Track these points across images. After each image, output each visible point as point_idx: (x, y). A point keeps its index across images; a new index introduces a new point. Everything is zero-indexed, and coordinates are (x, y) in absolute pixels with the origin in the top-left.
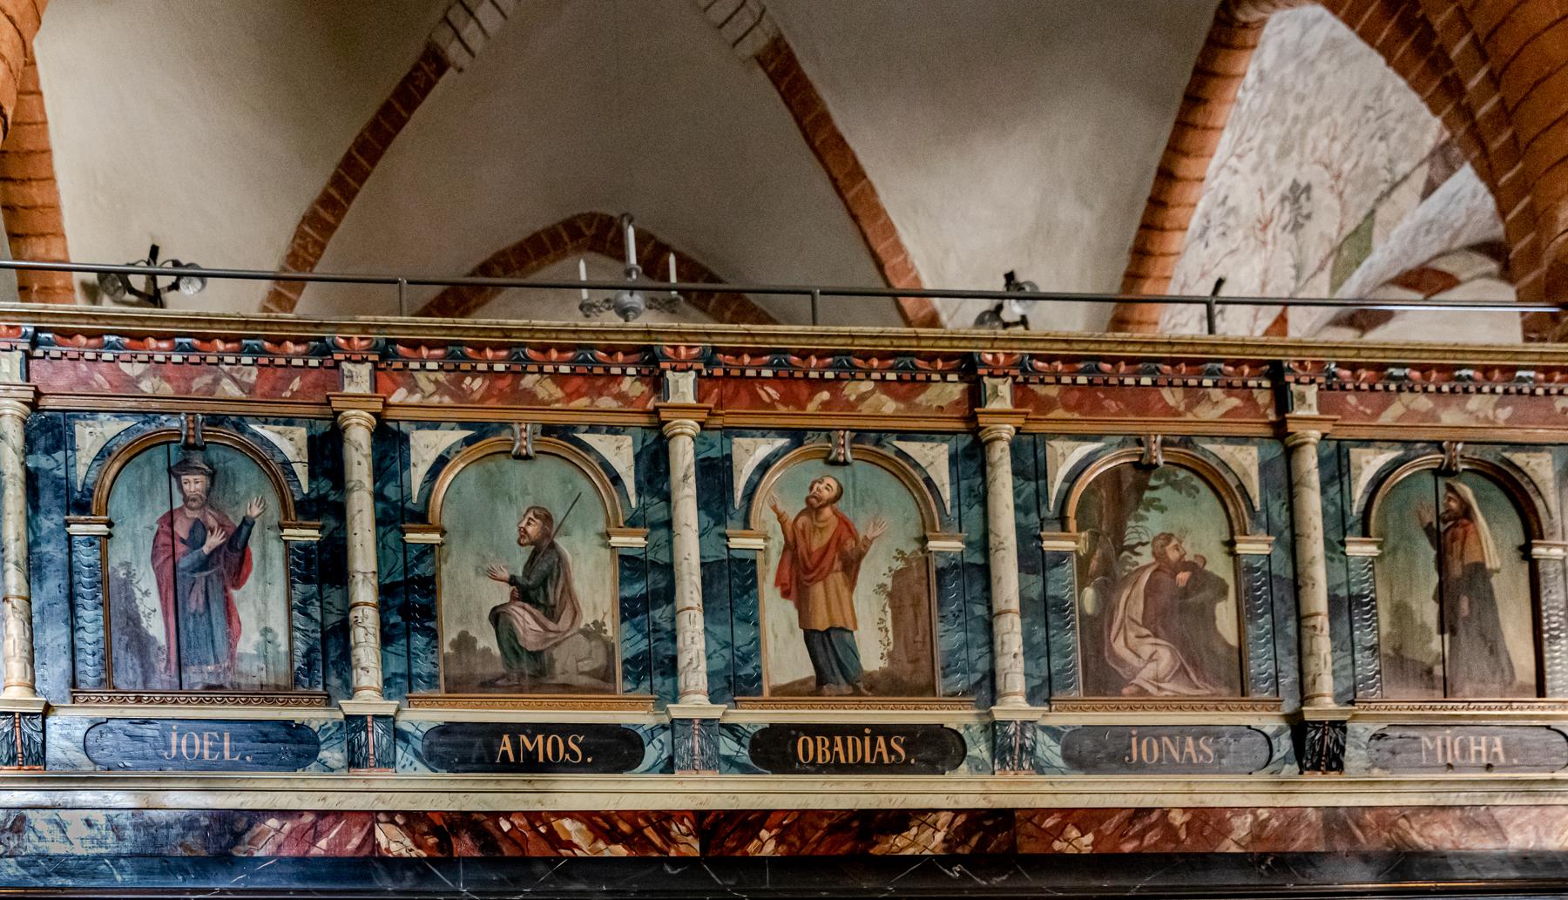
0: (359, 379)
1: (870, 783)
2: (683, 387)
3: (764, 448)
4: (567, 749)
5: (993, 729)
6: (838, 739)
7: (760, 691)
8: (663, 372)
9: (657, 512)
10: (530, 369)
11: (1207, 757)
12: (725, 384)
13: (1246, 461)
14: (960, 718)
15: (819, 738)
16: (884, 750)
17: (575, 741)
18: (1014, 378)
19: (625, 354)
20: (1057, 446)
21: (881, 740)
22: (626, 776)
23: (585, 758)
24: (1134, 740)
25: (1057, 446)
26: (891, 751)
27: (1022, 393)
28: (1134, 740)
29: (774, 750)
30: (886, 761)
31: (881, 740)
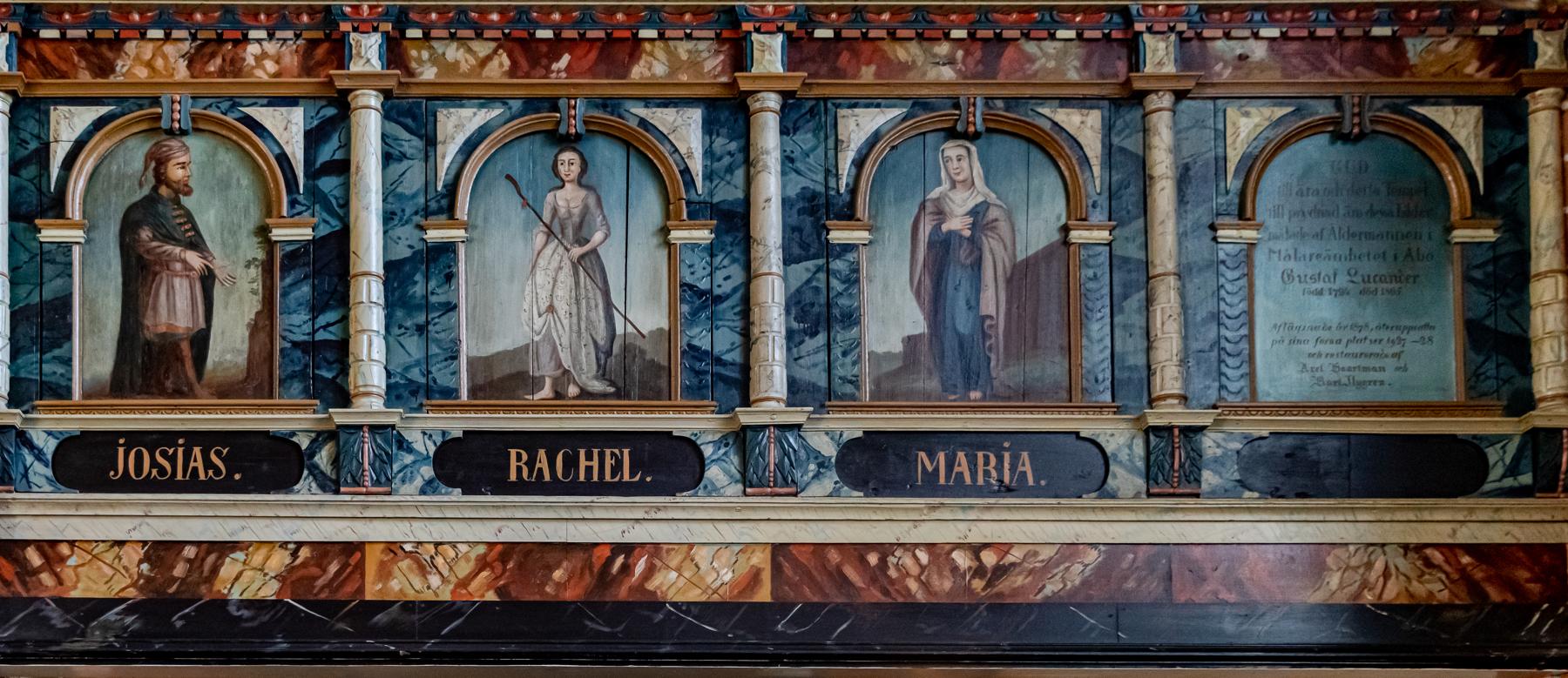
0: (368, 51)
1: (1471, 510)
2: (769, 55)
3: (86, 116)
4: (154, 464)
5: (742, 439)
6: (542, 453)
7: (66, 392)
8: (345, 35)
9: (728, 192)
10: (253, 34)
11: (218, 472)
12: (580, 52)
13: (1086, 126)
14: (698, 424)
15: (980, 454)
16: (200, 465)
17: (218, 453)
18: (1180, 33)
19: (694, 14)
20: (58, 114)
21: (197, 450)
22: (682, 498)
23: (230, 474)
24: (121, 450)
25: (58, 114)
26: (208, 464)
27: (394, 52)
28: (121, 450)
29: (875, 465)
30: (202, 477)
31: (197, 450)
